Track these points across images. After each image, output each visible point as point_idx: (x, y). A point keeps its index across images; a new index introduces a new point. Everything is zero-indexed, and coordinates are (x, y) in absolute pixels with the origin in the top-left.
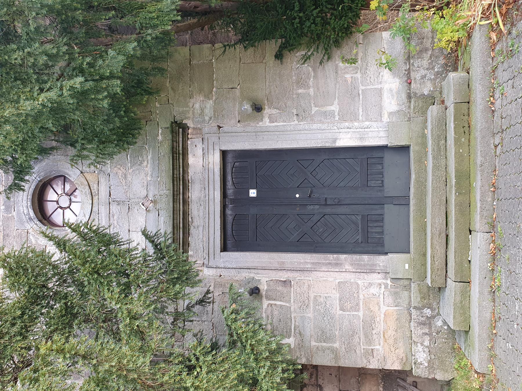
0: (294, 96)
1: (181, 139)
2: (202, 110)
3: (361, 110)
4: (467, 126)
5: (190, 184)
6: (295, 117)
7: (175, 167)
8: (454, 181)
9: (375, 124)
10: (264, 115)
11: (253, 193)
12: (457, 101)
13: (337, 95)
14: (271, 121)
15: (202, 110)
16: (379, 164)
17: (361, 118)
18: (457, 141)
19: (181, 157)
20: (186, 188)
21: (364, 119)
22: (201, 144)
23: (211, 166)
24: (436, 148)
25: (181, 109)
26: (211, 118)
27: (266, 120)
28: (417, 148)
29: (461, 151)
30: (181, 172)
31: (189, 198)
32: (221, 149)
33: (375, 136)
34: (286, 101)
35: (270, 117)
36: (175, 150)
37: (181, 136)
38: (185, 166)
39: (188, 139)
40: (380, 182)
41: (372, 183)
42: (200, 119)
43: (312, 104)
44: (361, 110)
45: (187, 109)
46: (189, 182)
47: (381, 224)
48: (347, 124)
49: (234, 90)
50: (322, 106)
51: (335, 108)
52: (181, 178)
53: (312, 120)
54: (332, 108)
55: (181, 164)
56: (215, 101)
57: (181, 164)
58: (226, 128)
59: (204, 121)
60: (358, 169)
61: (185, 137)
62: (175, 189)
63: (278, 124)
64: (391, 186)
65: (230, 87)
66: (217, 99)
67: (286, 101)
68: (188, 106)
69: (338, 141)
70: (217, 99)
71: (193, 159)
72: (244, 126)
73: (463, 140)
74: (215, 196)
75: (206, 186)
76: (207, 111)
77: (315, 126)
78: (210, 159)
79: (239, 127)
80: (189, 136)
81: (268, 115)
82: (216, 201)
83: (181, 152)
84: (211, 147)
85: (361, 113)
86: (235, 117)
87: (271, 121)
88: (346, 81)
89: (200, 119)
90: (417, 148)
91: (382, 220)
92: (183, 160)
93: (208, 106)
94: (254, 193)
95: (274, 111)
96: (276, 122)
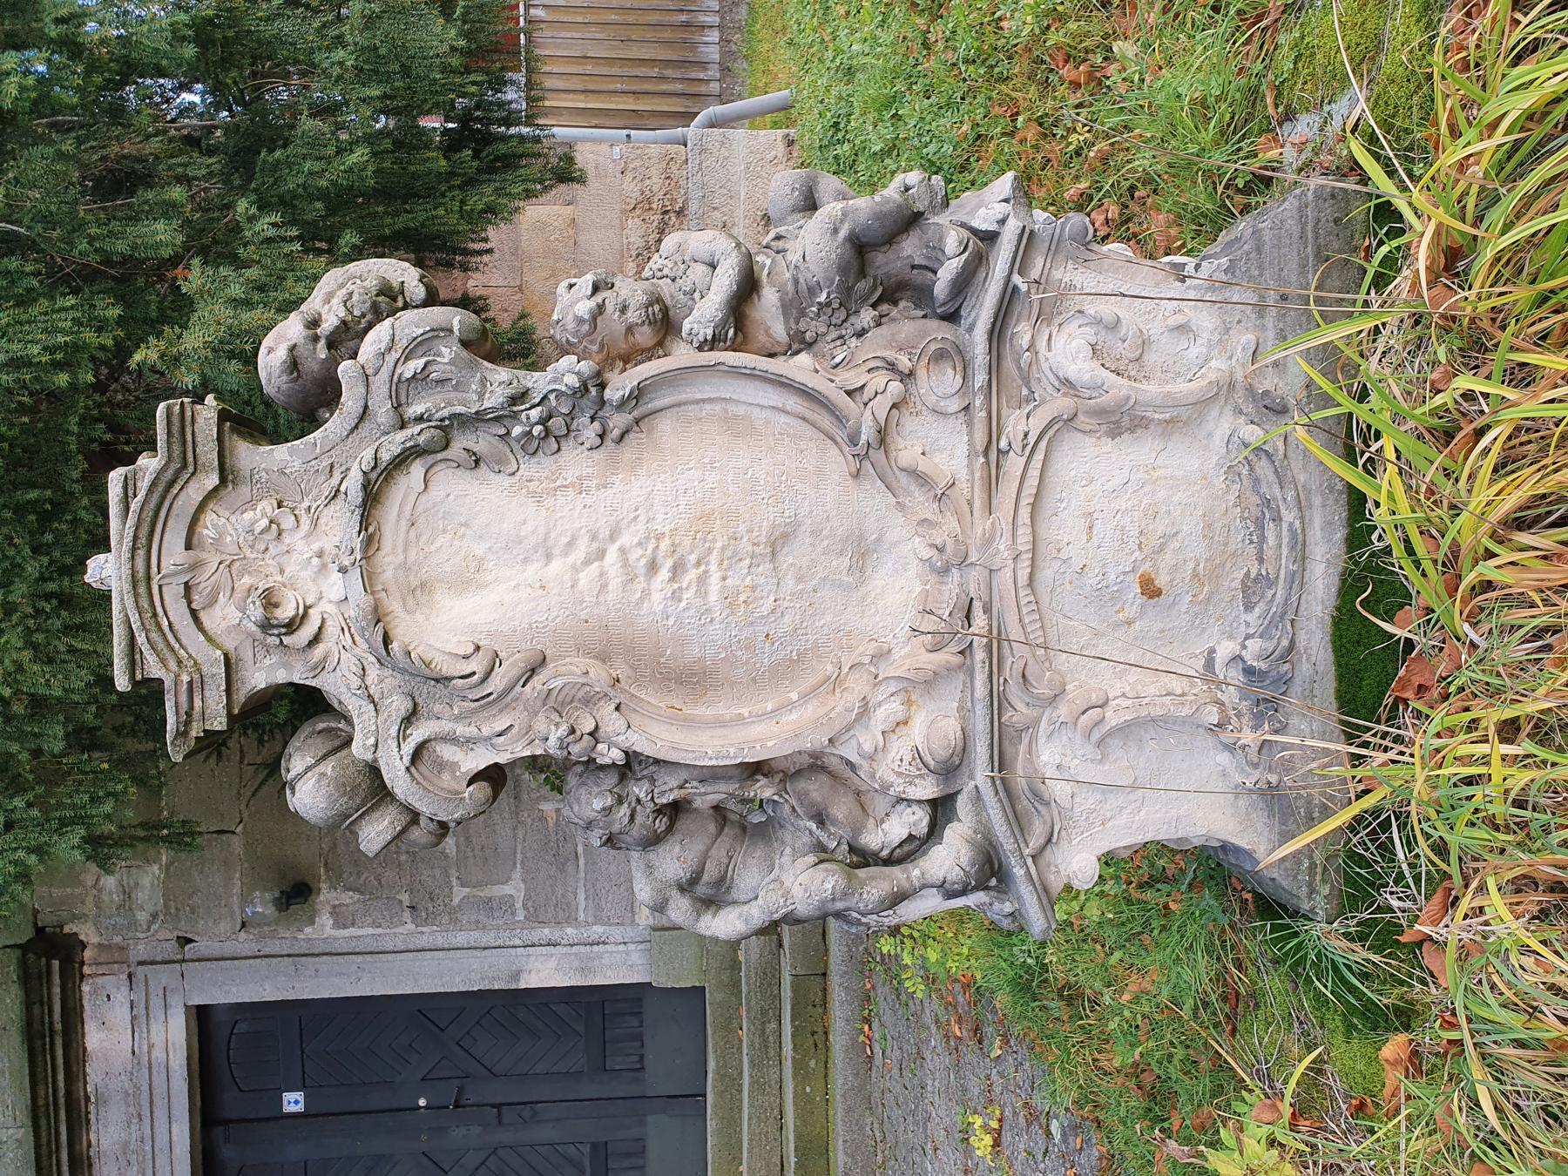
0: (403, 857)
1: (57, 990)
2: (127, 894)
3: (581, 896)
4: (820, 1030)
5: (92, 1108)
6: (407, 914)
7: (41, 1076)
8: (793, 1160)
9: (617, 933)
10: (318, 907)
11: (293, 1102)
12: (799, 971)
13: (519, 856)
14: (338, 925)
15: (127, 894)
16: (631, 1014)
17: (582, 916)
18: (799, 1066)
19: (59, 1042)
20: (78, 1119)
21: (590, 920)
22: (125, 990)
23: (158, 1053)
24: (757, 1041)
25: (56, 893)
26: (154, 916)
27: (325, 921)
28: (719, 996)
29: (808, 1089)
30: (61, 1084)
31: (89, 1145)
32: (190, 1003)
33: (620, 963)
34: (379, 870)
35: (335, 911)
36: (36, 1026)
37: (56, 980)
38: (75, 1056)
39: (82, 976)
40: (636, 1058)
41: (615, 1062)
42: (120, 920)
43: (454, 880)
44: (581, 896)
45: (78, 891)
46: (87, 1099)
47: (640, 1162)
48: (546, 931)
49: (224, 837)
50: (480, 884)
51: (514, 888)
52: (62, 1101)
53: (454, 921)
54: (507, 889)
55: (60, 1061)
56: (168, 867)
57: (60, 1061)
58: (202, 946)
59: (133, 924)
60: (580, 1029)
61: (72, 973)
62: (44, 1140)
63: (361, 932)
64: (660, 1077)
65: (213, 828)
66: (172, 863)
67: (379, 870)
68: (81, 884)
69: (524, 976)
70: (172, 863)
71: (102, 1035)
72: (261, 937)
73: (812, 1063)
74: (175, 1138)
75: (144, 1106)
76: (142, 896)
77: (461, 938)
78: (153, 1033)
79: (245, 943)
80: (86, 970)
81: (328, 908)
82: (177, 1150)
83: (58, 1027)
84: (157, 1002)
85: (582, 904)
86: (232, 913)
87: (338, 925)
88: (543, 819)
89: (120, 920)
90: (719, 996)
91: (643, 1152)
92: (66, 1047)
93: (146, 881)
94: (296, 1102)
95: (347, 898)
96: (353, 924)
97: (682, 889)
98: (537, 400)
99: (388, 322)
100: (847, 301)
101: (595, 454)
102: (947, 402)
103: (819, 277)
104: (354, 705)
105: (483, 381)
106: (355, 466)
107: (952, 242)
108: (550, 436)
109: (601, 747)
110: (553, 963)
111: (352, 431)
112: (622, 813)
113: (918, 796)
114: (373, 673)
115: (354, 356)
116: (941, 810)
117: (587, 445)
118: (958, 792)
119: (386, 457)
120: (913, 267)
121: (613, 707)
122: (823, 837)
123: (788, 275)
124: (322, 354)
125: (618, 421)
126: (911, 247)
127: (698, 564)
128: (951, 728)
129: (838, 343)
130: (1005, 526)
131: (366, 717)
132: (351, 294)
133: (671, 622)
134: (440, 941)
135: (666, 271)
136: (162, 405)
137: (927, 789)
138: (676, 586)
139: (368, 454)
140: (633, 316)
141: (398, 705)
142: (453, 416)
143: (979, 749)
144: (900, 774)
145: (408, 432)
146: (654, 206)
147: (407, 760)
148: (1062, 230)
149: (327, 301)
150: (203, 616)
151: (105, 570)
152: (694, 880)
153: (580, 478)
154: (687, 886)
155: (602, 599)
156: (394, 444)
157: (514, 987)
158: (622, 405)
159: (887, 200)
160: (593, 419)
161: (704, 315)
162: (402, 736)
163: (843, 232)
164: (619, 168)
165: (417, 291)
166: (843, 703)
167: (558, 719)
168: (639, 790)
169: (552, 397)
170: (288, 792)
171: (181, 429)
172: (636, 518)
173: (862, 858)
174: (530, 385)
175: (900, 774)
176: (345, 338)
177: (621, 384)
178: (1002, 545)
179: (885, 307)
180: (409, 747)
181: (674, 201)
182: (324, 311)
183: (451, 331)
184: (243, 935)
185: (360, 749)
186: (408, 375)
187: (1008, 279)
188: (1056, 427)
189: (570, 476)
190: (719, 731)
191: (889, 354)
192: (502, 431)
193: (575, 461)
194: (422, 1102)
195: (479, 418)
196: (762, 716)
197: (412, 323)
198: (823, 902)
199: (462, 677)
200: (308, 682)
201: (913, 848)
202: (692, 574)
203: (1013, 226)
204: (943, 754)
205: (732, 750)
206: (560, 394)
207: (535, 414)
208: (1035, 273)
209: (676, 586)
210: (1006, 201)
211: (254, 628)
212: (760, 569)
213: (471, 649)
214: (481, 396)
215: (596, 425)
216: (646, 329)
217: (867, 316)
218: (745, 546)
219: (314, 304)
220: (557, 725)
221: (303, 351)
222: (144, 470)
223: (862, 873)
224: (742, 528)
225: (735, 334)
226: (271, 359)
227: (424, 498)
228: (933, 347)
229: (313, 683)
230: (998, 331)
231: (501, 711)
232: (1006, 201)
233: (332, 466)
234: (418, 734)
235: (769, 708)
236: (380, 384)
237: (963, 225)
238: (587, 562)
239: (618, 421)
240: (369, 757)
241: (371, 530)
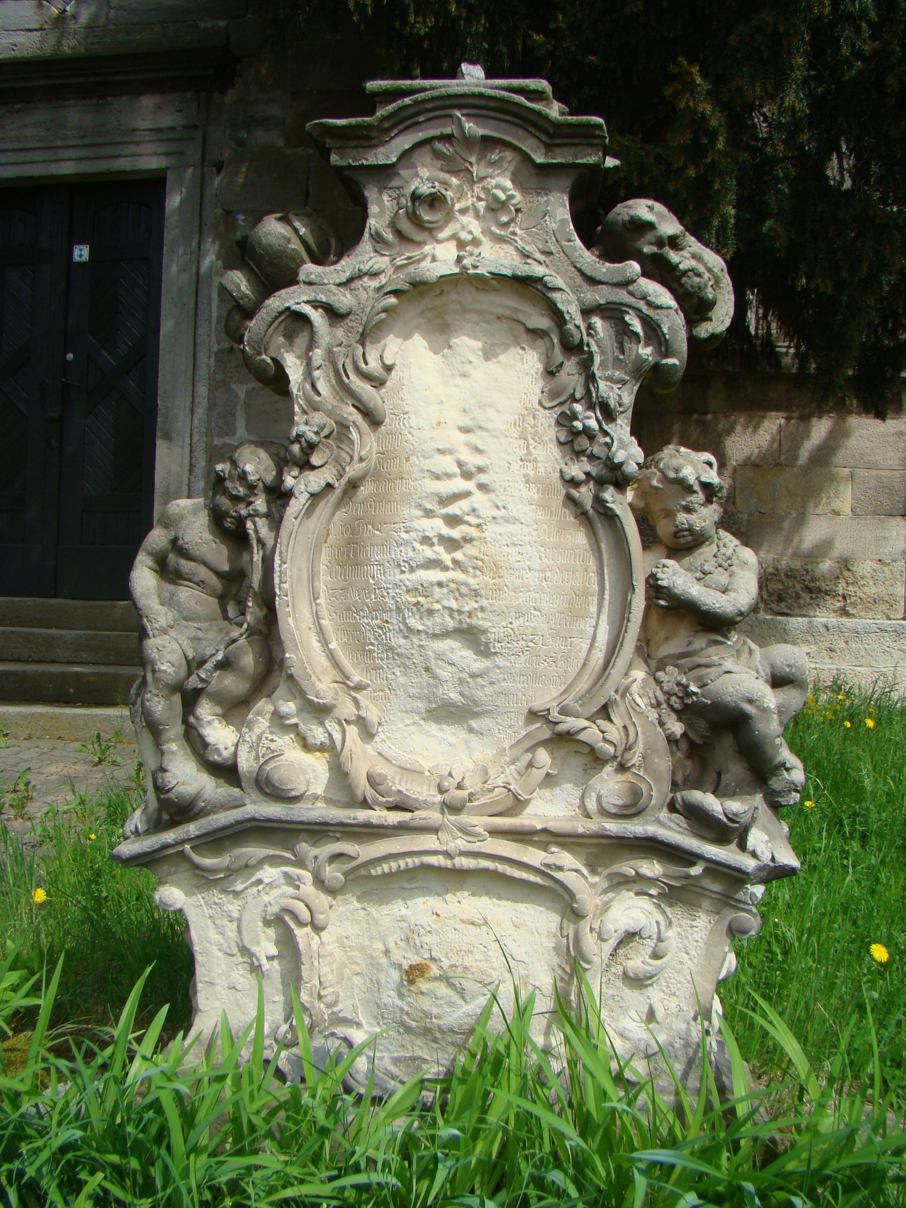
77: (202, 391)
94: (81, 256)
97: (174, 541)
98: (605, 427)
99: (673, 303)
100: (688, 709)
101: (558, 475)
102: (594, 799)
103: (712, 687)
104: (346, 266)
105: (623, 382)
106: (547, 272)
107: (735, 806)
108: (573, 441)
109: (295, 472)
110: (175, 468)
111: (580, 271)
112: (241, 489)
113: (240, 753)
114: (374, 284)
115: (645, 274)
116: (227, 771)
117: (565, 468)
118: (242, 789)
119: (556, 296)
120: (719, 774)
121: (331, 481)
122: (209, 665)
123: (715, 658)
124: (647, 249)
125: (585, 494)
126: (735, 771)
127: (455, 562)
128: (297, 786)
129: (654, 701)
130: (478, 846)
131: (335, 276)
132: (699, 275)
133: (404, 536)
134: (203, 372)
135: (723, 550)
136: (601, 121)
137: (246, 763)
138: (435, 540)
139: (559, 282)
140: (682, 518)
141: (344, 300)
142: (591, 355)
143: (272, 809)
144: (260, 738)
145: (579, 321)
146: (850, 588)
147: (296, 308)
148: (744, 910)
149: (694, 256)
150: (426, 149)
151: (473, 76)
152: (184, 553)
153: (535, 461)
154: (176, 546)
155: (426, 474)
156: (569, 304)
157: (158, 434)
158: (599, 501)
159: (777, 748)
160: (588, 474)
161: (677, 577)
162: (316, 304)
163: (749, 709)
164: (884, 558)
165: (704, 330)
166: (324, 687)
167: (322, 434)
168: (260, 503)
169: (608, 440)
170: (279, 215)
171: (582, 136)
172: (498, 507)
173: (190, 699)
174: (619, 421)
175: (260, 738)
176: (660, 269)
177: (621, 503)
178: (461, 843)
179: (684, 745)
180: (307, 309)
181: (854, 605)
182: (685, 253)
183: (667, 356)
184: (219, 212)
185: (309, 269)
186: (627, 318)
187: (700, 857)
188: (567, 897)
189: (539, 452)
190: (305, 575)
191: (640, 748)
192: (578, 395)
193: (549, 457)
194: (70, 356)
195: (590, 378)
196: (317, 617)
197: (673, 322)
198: (153, 663)
199: (364, 354)
200: (367, 230)
201: (198, 745)
202: (441, 553)
203: (749, 864)
204: (275, 777)
205: (286, 586)
206: (609, 446)
207: (593, 423)
208: (708, 883)
209: (435, 540)
210: (773, 859)
211: (413, 188)
212: (448, 619)
213: (388, 362)
214: (609, 379)
215: (583, 477)
216: (672, 529)
217: (677, 728)
218: (470, 605)
219: (693, 244)
220: (317, 433)
221: (650, 236)
222: (549, 105)
223: (177, 699)
224: (484, 603)
225: (662, 607)
226: (643, 209)
227: (522, 328)
228: (644, 788)
229: (366, 235)
230: (653, 847)
231: (333, 387)
232: (773, 859)
233: (551, 253)
234: (316, 317)
235: (322, 621)
236: (622, 296)
237: (753, 819)
238: (460, 464)
239: (585, 494)
240: (302, 277)
241: (494, 283)
